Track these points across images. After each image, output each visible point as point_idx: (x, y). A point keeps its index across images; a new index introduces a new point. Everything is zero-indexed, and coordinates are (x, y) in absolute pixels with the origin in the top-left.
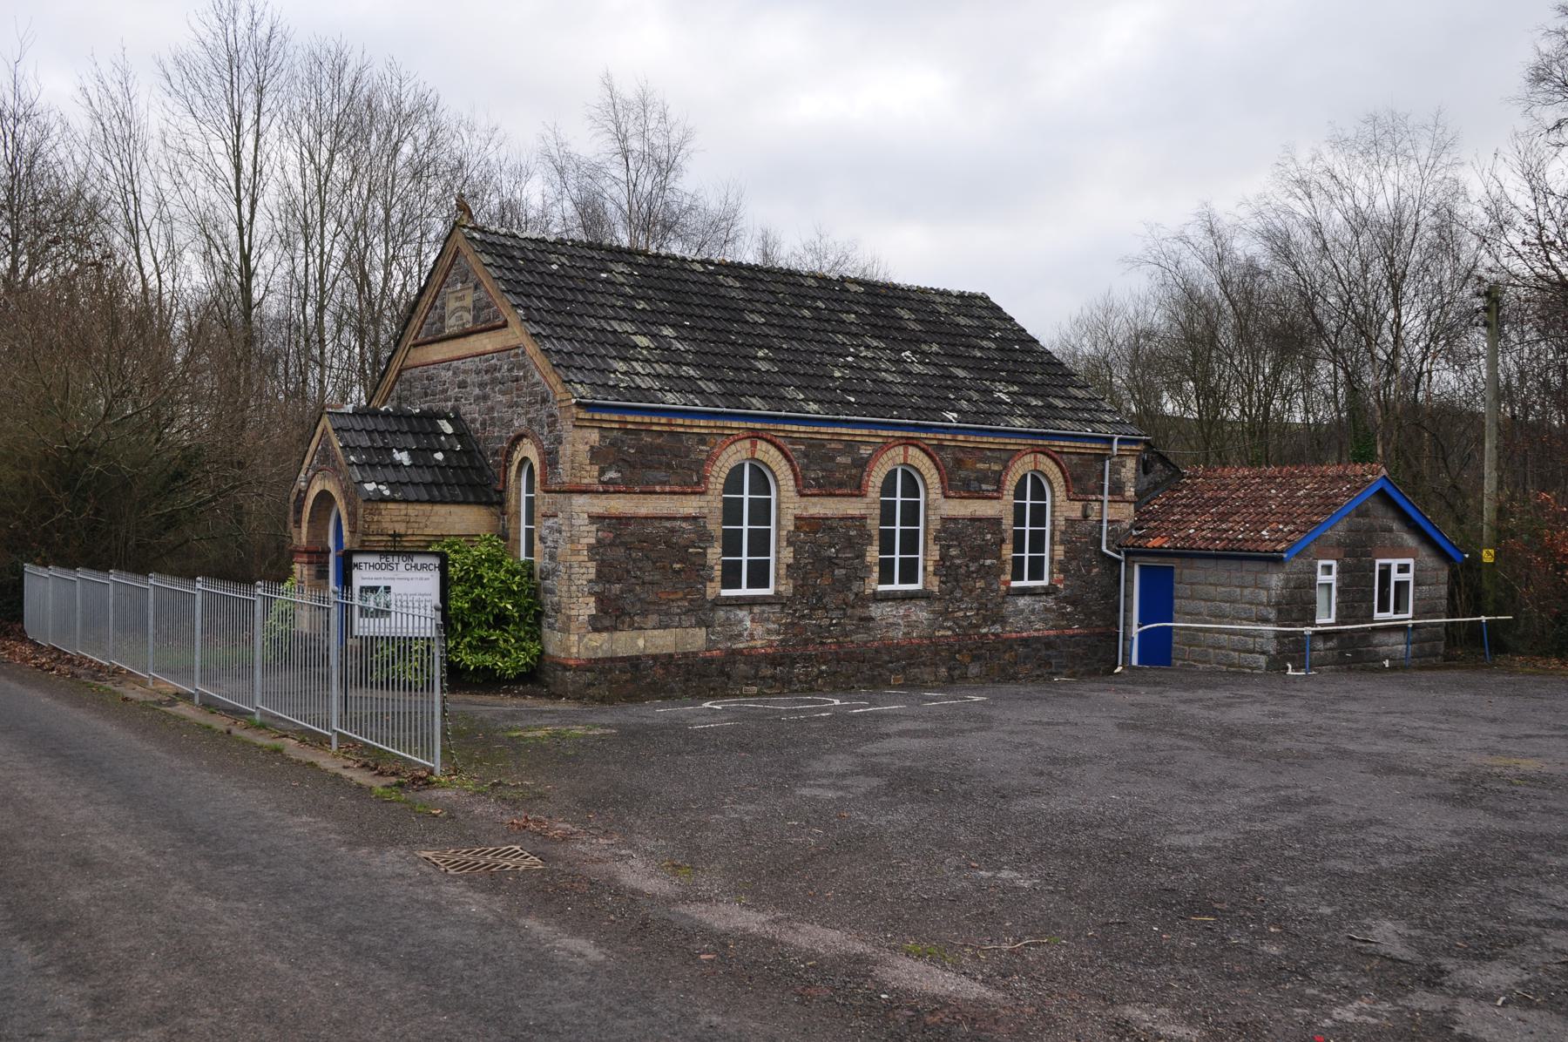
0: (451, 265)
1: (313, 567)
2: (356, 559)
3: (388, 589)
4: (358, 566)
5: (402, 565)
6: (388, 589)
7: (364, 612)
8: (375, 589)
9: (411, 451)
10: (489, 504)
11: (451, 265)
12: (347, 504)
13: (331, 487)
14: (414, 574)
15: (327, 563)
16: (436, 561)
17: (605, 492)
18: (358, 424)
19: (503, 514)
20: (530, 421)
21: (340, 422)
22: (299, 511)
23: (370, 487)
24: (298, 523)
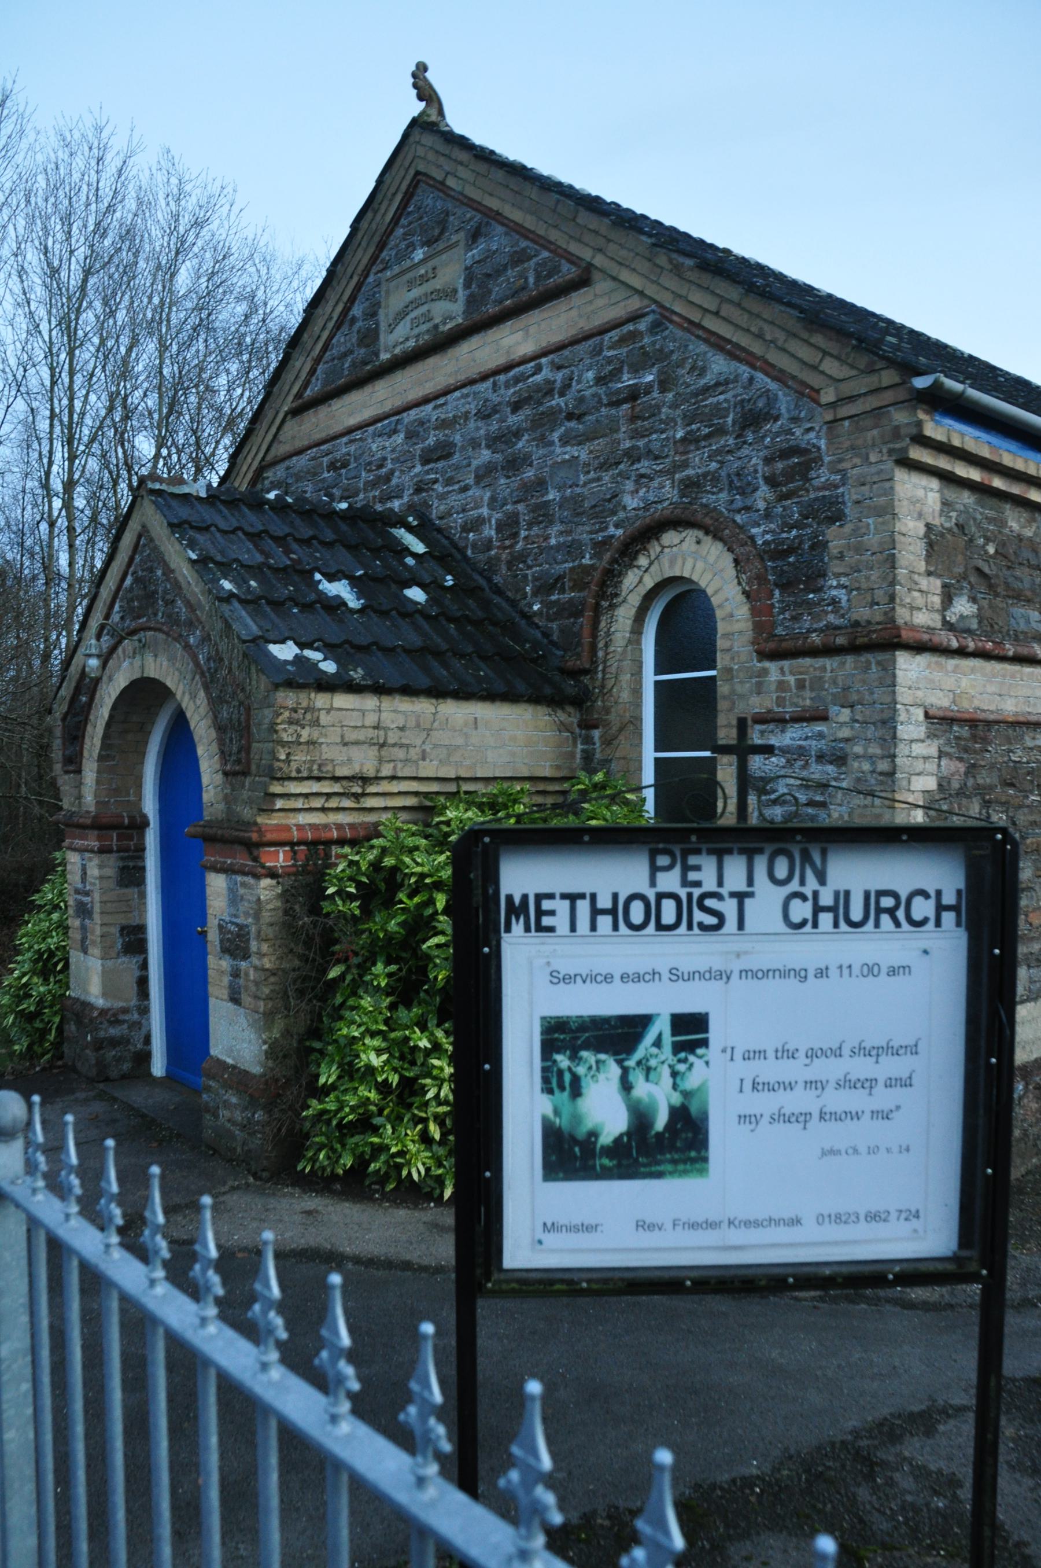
0: (395, 221)
1: (112, 860)
2: (520, 877)
3: (691, 1030)
4: (532, 913)
5: (767, 900)
6: (691, 1030)
7: (569, 1154)
8: (619, 1035)
9: (355, 582)
10: (554, 701)
11: (395, 221)
12: (215, 703)
13: (159, 667)
14: (828, 946)
15: (141, 849)
16: (940, 876)
17: (961, 652)
18: (225, 519)
19: (587, 725)
20: (690, 486)
21: (184, 512)
22: (75, 735)
23: (285, 652)
24: (74, 763)
